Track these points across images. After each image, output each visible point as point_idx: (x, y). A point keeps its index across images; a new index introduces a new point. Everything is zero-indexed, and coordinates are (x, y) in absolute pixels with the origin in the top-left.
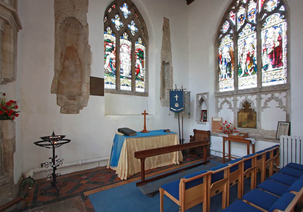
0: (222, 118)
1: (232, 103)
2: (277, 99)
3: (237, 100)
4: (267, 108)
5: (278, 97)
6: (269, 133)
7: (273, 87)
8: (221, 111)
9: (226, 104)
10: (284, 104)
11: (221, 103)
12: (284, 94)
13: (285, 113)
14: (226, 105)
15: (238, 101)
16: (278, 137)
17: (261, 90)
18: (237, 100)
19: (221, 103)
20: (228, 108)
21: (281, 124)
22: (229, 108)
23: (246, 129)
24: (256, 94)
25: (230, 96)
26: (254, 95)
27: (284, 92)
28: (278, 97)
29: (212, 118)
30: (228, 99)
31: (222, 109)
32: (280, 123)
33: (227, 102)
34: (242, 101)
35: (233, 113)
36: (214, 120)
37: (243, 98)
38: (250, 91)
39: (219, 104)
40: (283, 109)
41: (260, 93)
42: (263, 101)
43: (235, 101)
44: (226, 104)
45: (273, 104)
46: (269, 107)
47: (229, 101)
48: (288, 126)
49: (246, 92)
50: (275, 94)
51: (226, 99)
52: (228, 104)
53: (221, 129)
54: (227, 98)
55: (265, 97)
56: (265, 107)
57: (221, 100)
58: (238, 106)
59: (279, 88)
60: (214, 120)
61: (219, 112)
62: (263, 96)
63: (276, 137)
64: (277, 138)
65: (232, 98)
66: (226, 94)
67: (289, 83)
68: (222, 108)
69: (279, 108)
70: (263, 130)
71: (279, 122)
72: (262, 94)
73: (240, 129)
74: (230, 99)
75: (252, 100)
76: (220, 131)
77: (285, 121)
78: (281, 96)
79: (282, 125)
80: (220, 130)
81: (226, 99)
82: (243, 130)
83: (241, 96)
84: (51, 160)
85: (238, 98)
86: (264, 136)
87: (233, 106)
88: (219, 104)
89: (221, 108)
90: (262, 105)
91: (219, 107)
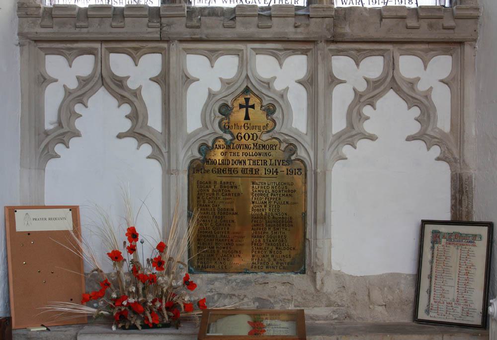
0: (74, 210)
1: (152, 97)
2: (412, 95)
3: (44, 80)
4: (362, 144)
5: (418, 79)
6: (376, 295)
7: (403, 18)
8: (68, 159)
9: (390, 101)
10: (443, 123)
11: (68, 92)
12: (442, 64)
13: (444, 172)
14: (102, 114)
15: (193, 86)
16: (427, 312)
17: (339, 30)
18: (44, 80)
19: (68, 92)
20: (120, 136)
21: (436, 234)
22: (131, 133)
23: (246, 283)
24: (304, 52)
25: (135, 47)
26: (295, 52)
27: (446, 52)
28: (418, 79)
29: (11, 211)
30: (120, 64)
31: (73, 142)
32: (429, 228)
33: (119, 88)
34: (278, 86)
35: (155, 169)
36: (20, 227)
37: (227, 66)
38: (279, 27)
39: (53, 98)
40: (436, 151)
41: (333, 46)
42: (341, 97)
43: (170, 83)
44: (102, 99)
45: (391, 116)
46: (372, 138)
47: (132, 85)
48: (481, 248)
49: (252, 30)
50: (401, 57)
51: (102, 63)
52: (122, 99)
53: (96, 296)
54: (113, 56)
55: (352, 72)
56: (353, 134)
57: (65, 71)
58: (193, 122)
59: (431, 26)
60: (20, 227)
61: (52, 165)
62: (341, 64)
63: (409, 310)
64: (422, 315)
65: (152, 63)
66: (107, 29)
67: (473, 5)
68: (77, 134)
69: (420, 144)
70: (339, 276)
71: (425, 223)
72: (339, 52)
73: (211, 282)
74: (140, 71)
75: (278, 86)
76: (87, 310)
77: (447, 217)
78: (429, 72)
79: (444, 241)
80: (86, 300)
81: (102, 63)
82: (226, 290)
83: (212, 56)
84: (453, 288)
85: (195, 64)
86: (352, 312)
87: (155, 121)
88: (53, 98)
89: (66, 133)
90: (338, 124)
91: (48, 126)
